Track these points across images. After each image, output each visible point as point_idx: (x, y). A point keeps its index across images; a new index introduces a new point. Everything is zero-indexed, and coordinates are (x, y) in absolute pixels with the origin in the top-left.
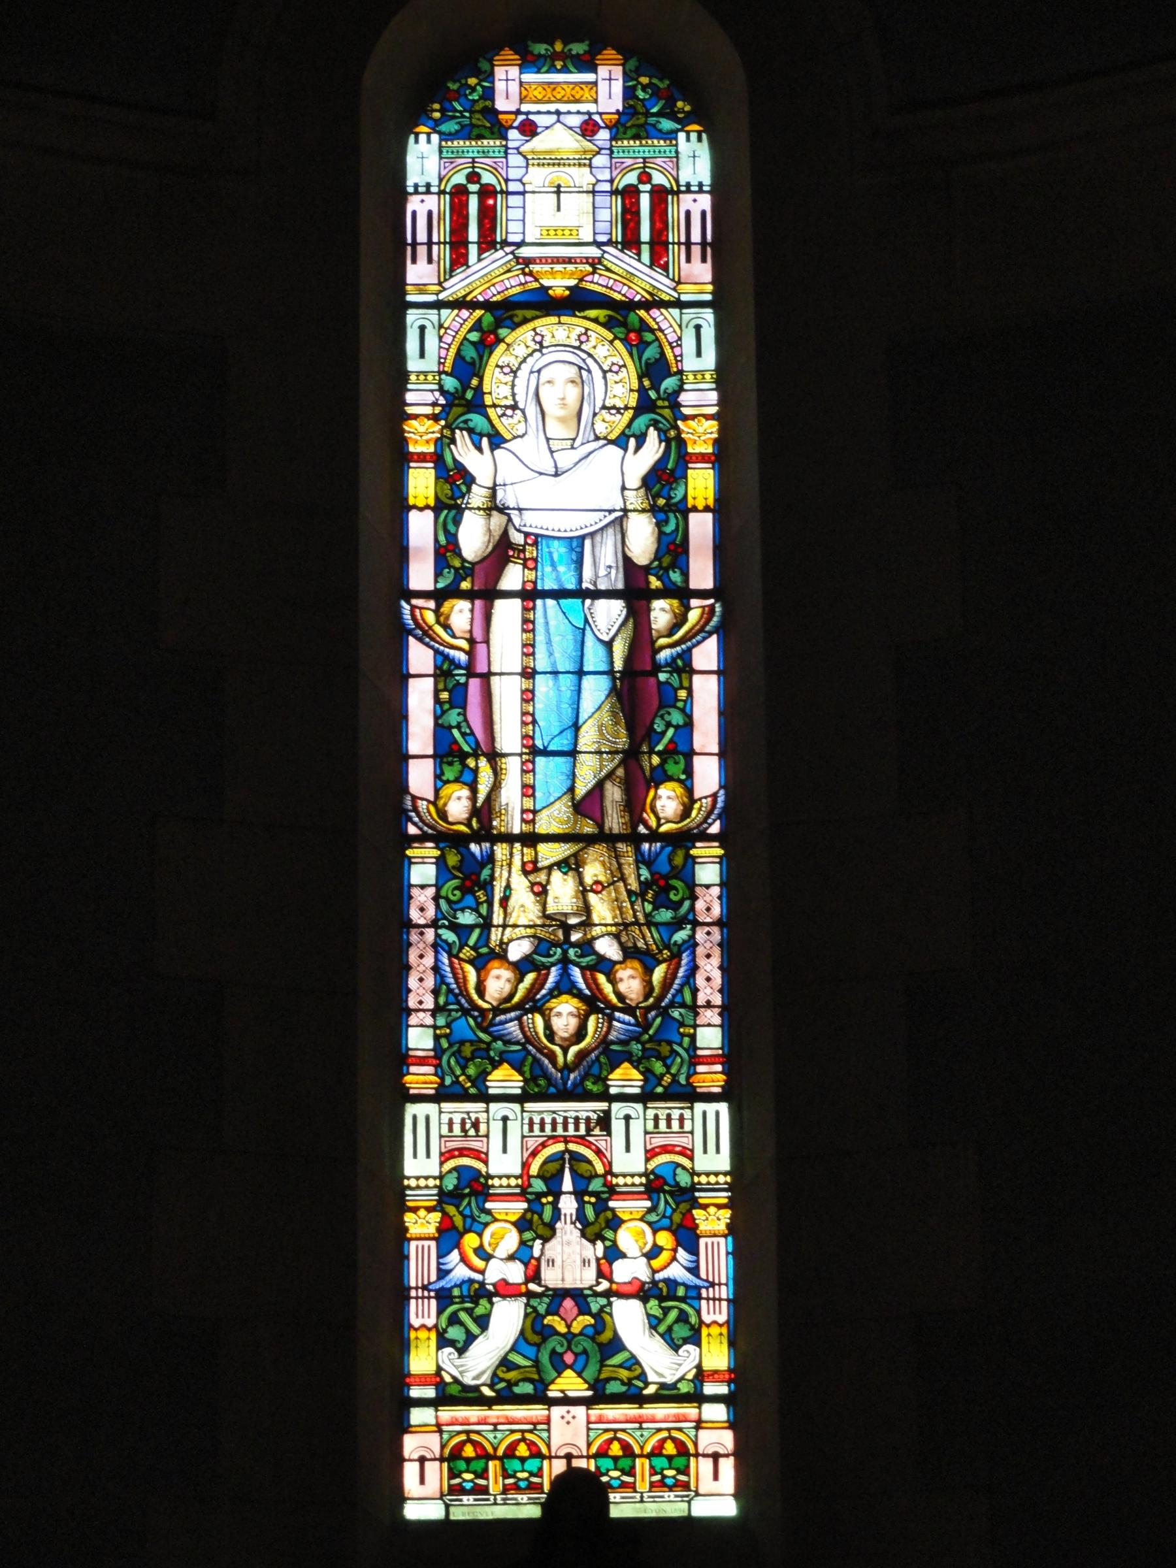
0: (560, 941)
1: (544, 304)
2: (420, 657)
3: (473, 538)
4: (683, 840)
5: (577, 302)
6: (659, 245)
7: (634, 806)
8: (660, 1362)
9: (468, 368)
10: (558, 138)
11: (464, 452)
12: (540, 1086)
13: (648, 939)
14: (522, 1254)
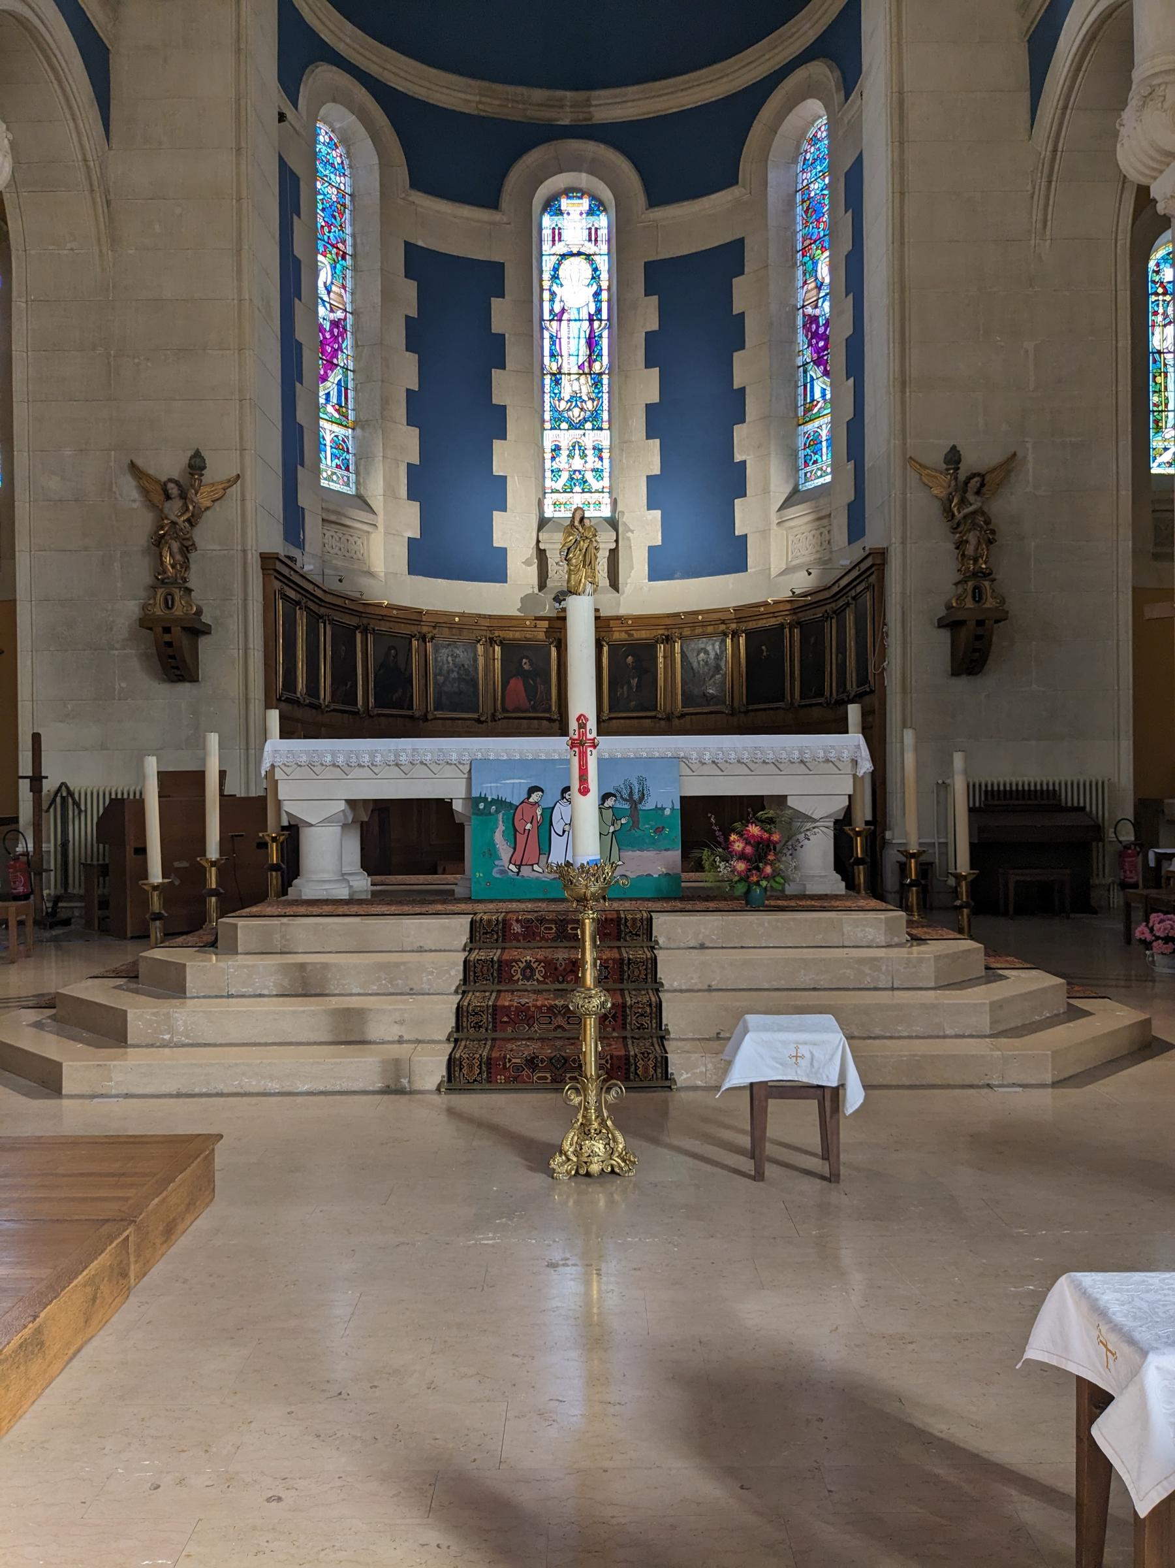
0: (575, 398)
1: (572, 255)
2: (546, 334)
3: (557, 309)
4: (601, 374)
5: (579, 254)
6: (596, 240)
7: (590, 367)
8: (596, 485)
9: (556, 269)
10: (575, 215)
11: (555, 288)
12: (572, 426)
13: (593, 396)
14: (568, 462)
